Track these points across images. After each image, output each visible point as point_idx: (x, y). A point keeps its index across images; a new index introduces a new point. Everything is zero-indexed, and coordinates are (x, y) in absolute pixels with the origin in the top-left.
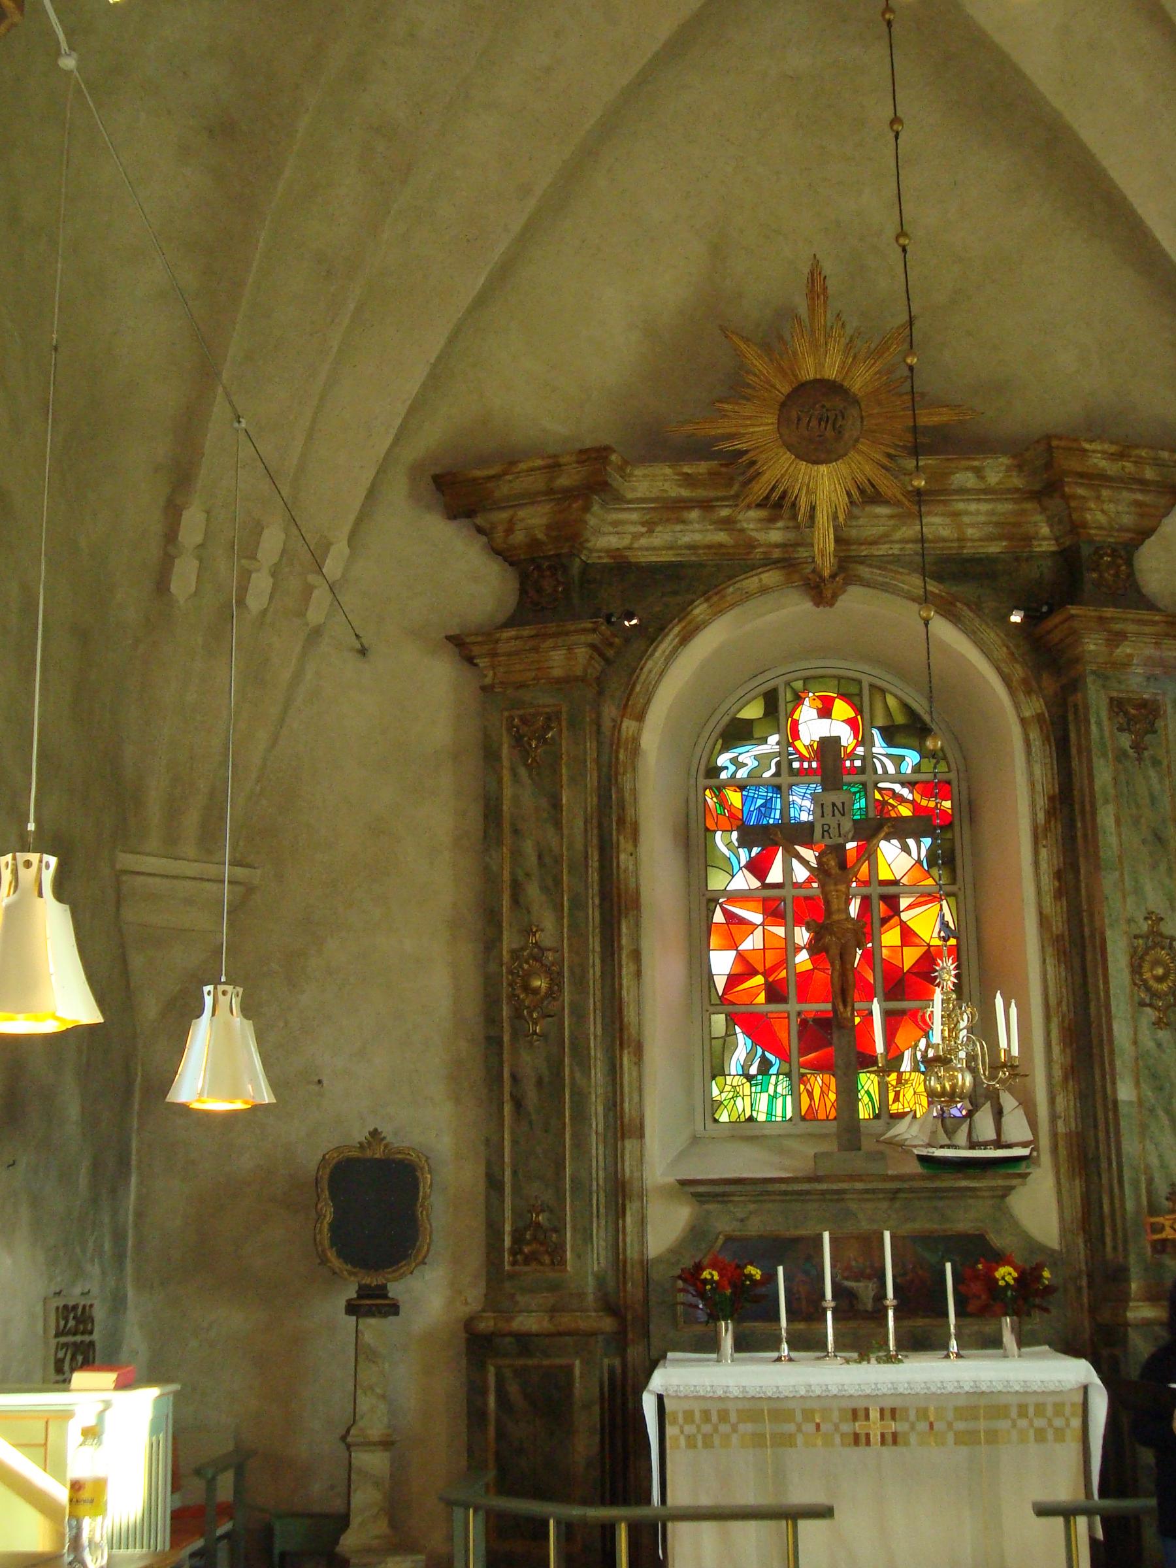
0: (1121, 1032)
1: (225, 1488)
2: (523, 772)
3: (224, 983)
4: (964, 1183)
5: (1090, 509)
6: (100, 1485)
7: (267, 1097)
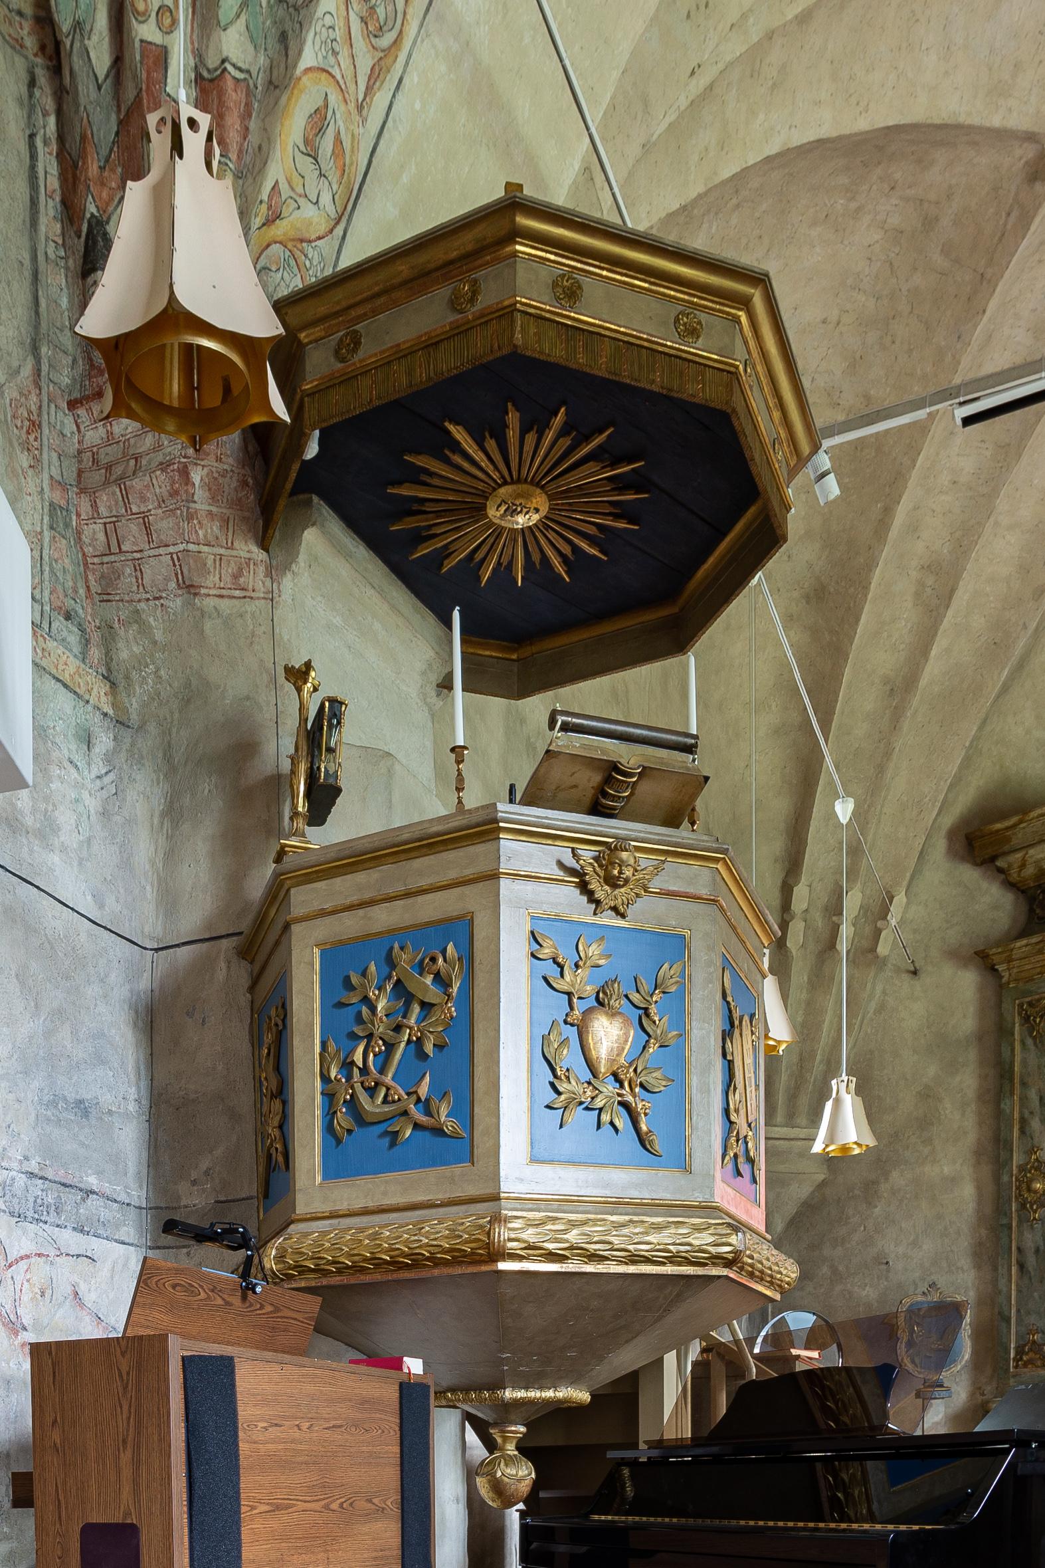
2: (1029, 1041)
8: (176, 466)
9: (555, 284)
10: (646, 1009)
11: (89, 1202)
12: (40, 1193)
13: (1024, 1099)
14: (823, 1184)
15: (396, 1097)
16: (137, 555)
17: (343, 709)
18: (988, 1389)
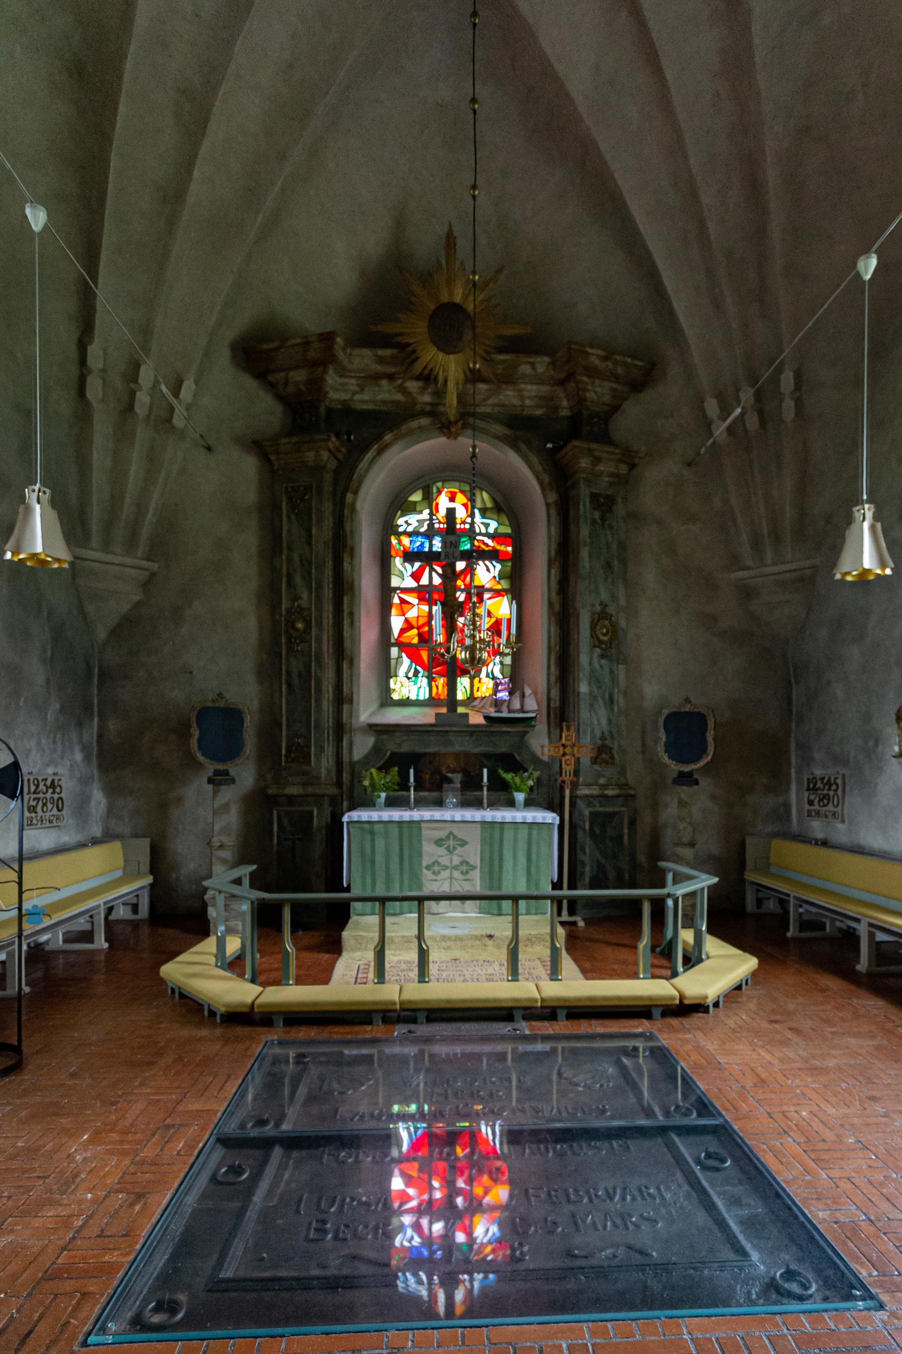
0: (584, 659)
2: (293, 517)
4: (504, 729)
5: (588, 390)
13: (290, 560)
14: (139, 604)
18: (269, 776)
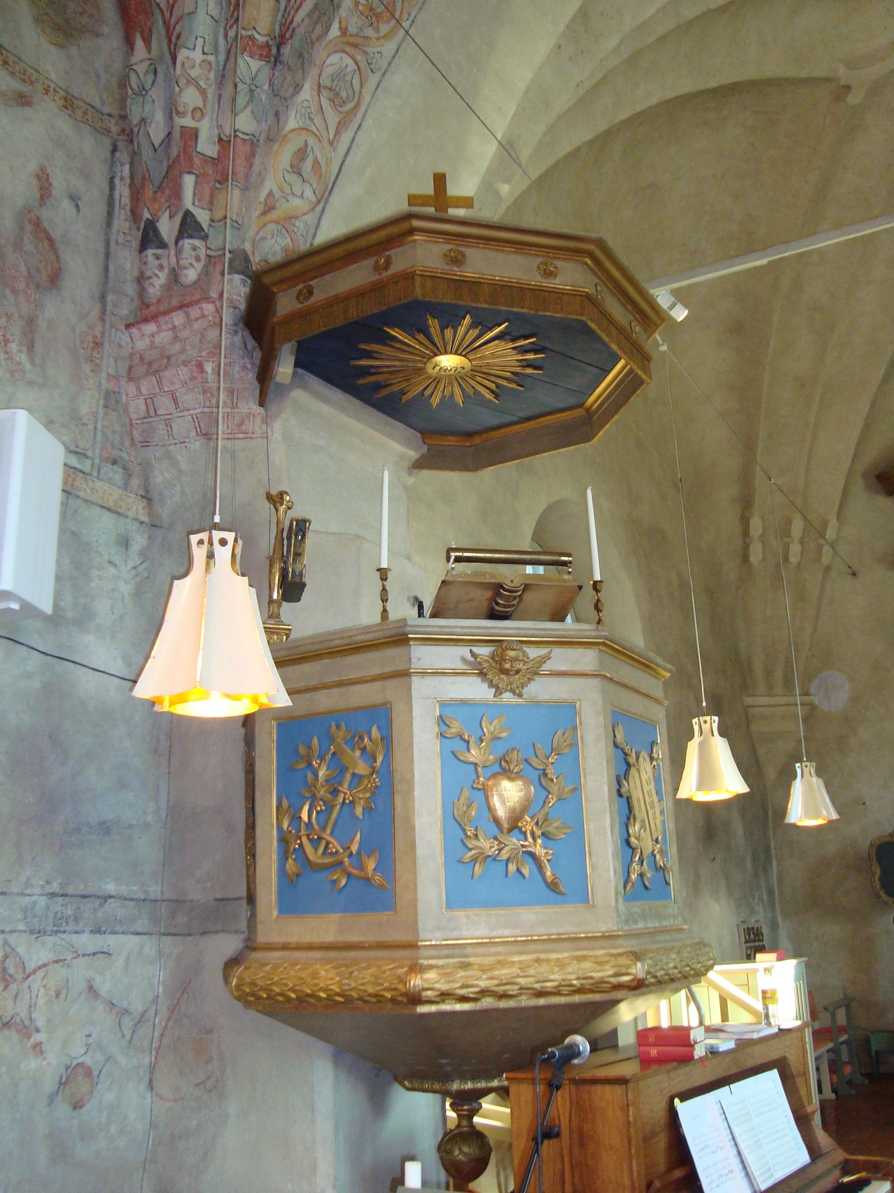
1: (841, 1018)
3: (806, 761)
6: (774, 992)
7: (835, 816)
8: (194, 363)
9: (445, 255)
10: (544, 770)
11: (107, 905)
12: (60, 909)
15: (334, 850)
16: (169, 417)
17: (307, 525)
